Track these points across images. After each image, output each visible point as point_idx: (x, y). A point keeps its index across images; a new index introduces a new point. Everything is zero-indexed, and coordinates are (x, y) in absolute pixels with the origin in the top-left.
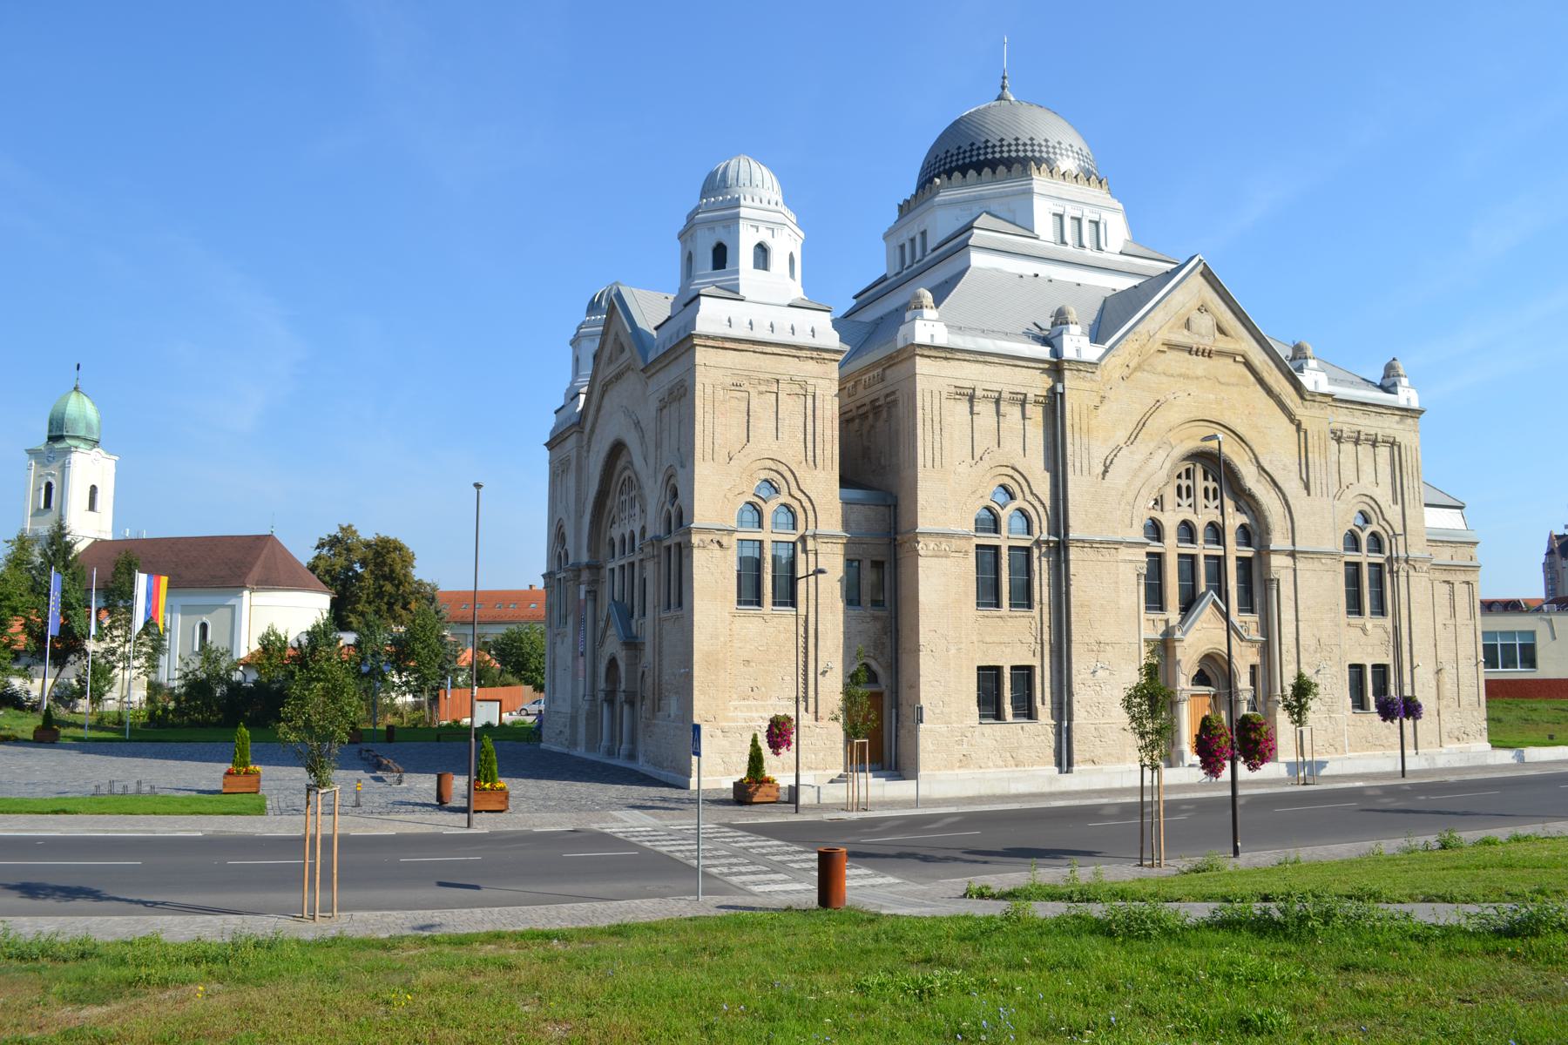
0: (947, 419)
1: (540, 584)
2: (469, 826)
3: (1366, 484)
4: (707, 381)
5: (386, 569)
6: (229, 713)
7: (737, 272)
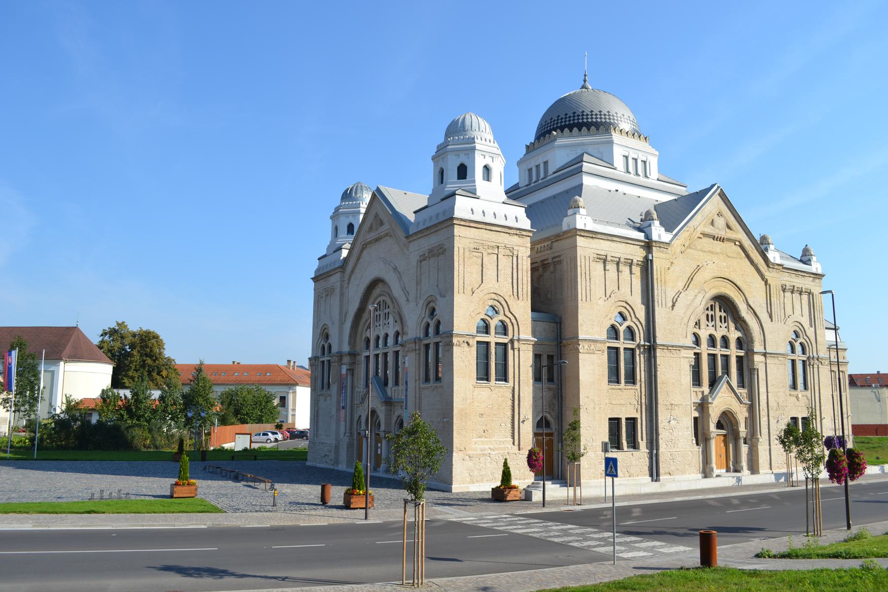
0: (593, 273)
1: (306, 364)
2: (366, 518)
3: (797, 316)
4: (460, 246)
5: (148, 350)
6: (80, 440)
7: (474, 181)
